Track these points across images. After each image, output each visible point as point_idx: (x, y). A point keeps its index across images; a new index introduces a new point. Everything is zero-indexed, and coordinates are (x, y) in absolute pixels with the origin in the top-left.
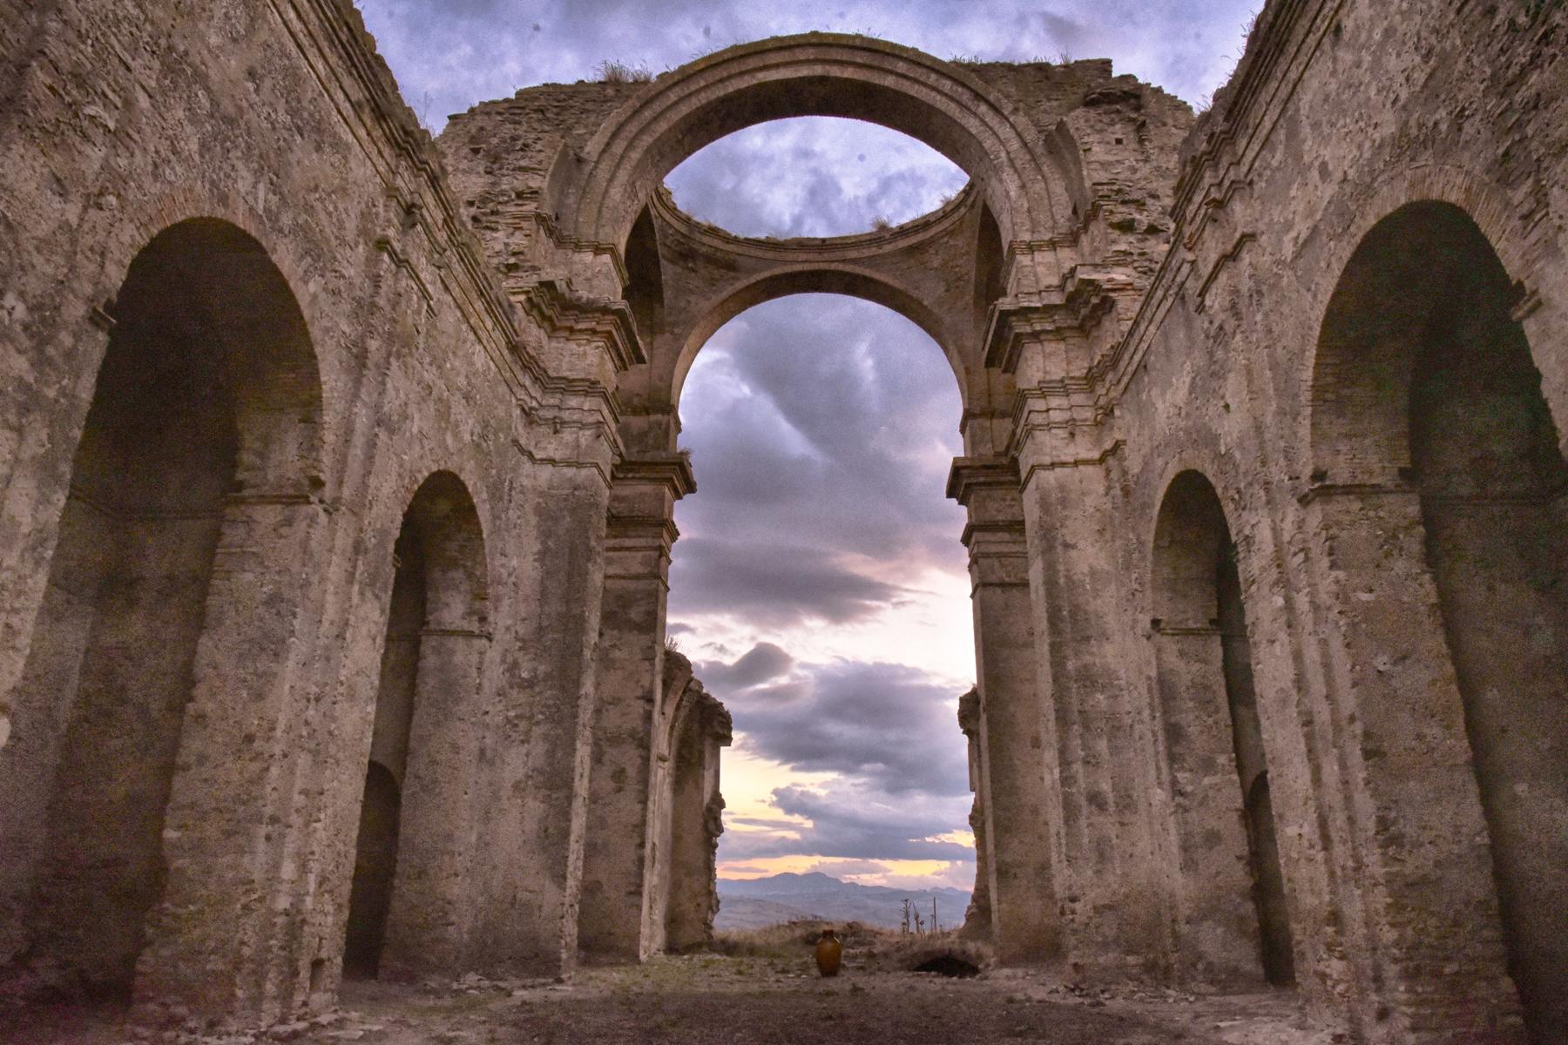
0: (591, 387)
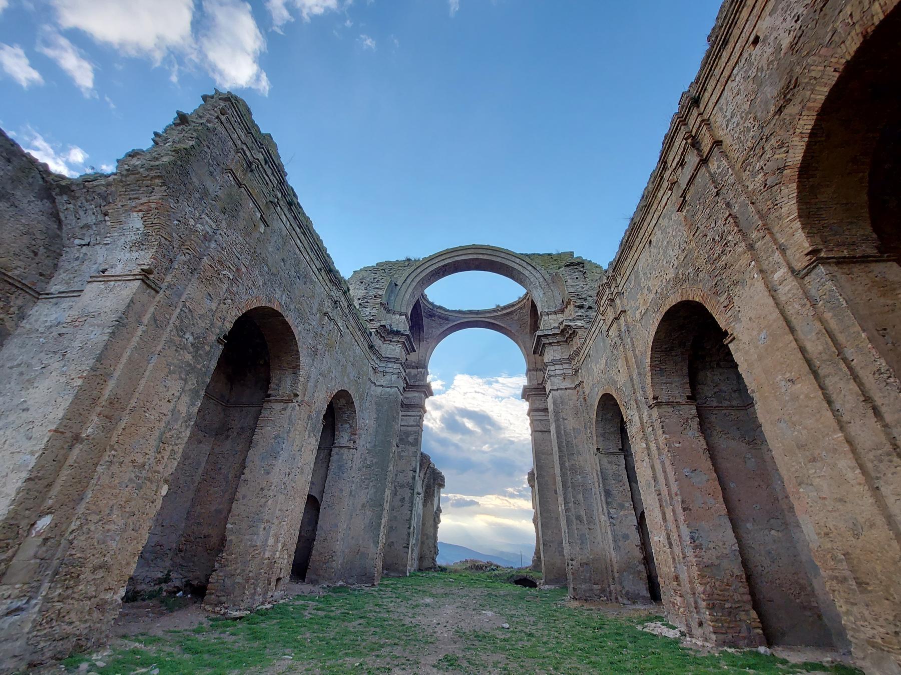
0: (396, 360)
